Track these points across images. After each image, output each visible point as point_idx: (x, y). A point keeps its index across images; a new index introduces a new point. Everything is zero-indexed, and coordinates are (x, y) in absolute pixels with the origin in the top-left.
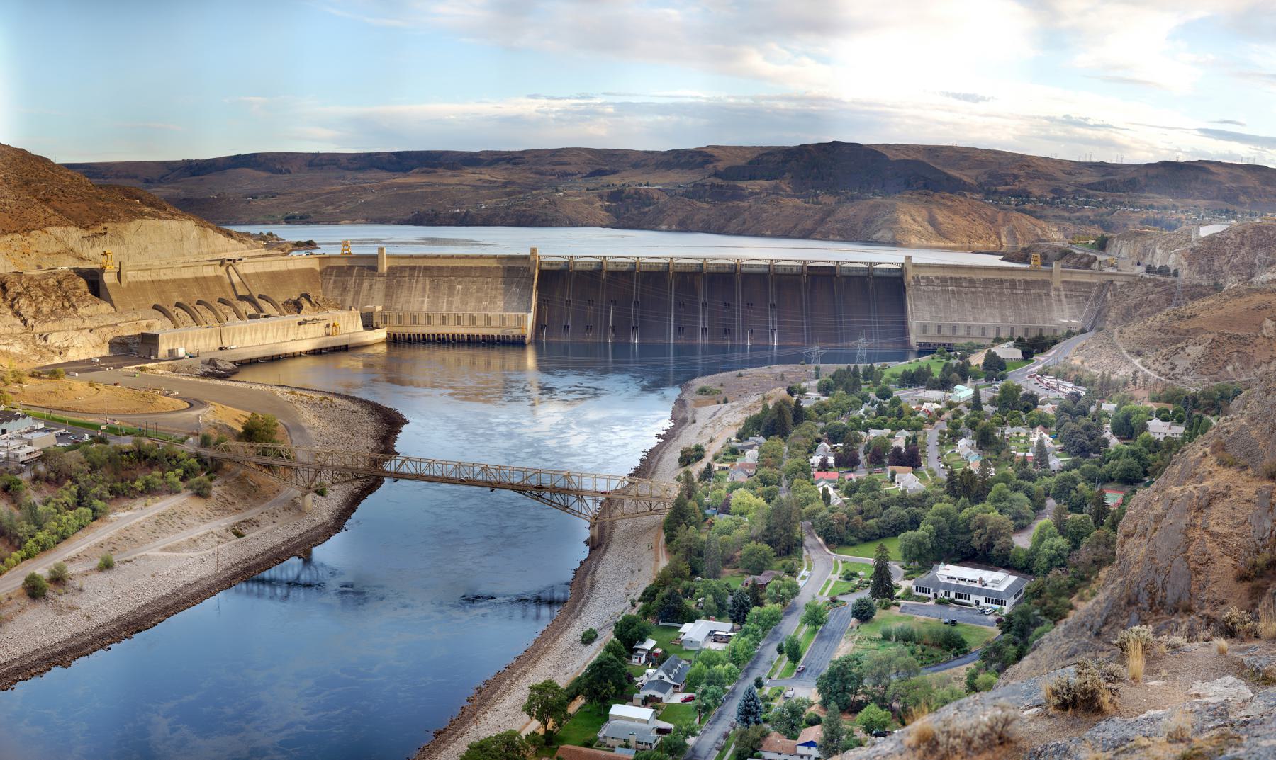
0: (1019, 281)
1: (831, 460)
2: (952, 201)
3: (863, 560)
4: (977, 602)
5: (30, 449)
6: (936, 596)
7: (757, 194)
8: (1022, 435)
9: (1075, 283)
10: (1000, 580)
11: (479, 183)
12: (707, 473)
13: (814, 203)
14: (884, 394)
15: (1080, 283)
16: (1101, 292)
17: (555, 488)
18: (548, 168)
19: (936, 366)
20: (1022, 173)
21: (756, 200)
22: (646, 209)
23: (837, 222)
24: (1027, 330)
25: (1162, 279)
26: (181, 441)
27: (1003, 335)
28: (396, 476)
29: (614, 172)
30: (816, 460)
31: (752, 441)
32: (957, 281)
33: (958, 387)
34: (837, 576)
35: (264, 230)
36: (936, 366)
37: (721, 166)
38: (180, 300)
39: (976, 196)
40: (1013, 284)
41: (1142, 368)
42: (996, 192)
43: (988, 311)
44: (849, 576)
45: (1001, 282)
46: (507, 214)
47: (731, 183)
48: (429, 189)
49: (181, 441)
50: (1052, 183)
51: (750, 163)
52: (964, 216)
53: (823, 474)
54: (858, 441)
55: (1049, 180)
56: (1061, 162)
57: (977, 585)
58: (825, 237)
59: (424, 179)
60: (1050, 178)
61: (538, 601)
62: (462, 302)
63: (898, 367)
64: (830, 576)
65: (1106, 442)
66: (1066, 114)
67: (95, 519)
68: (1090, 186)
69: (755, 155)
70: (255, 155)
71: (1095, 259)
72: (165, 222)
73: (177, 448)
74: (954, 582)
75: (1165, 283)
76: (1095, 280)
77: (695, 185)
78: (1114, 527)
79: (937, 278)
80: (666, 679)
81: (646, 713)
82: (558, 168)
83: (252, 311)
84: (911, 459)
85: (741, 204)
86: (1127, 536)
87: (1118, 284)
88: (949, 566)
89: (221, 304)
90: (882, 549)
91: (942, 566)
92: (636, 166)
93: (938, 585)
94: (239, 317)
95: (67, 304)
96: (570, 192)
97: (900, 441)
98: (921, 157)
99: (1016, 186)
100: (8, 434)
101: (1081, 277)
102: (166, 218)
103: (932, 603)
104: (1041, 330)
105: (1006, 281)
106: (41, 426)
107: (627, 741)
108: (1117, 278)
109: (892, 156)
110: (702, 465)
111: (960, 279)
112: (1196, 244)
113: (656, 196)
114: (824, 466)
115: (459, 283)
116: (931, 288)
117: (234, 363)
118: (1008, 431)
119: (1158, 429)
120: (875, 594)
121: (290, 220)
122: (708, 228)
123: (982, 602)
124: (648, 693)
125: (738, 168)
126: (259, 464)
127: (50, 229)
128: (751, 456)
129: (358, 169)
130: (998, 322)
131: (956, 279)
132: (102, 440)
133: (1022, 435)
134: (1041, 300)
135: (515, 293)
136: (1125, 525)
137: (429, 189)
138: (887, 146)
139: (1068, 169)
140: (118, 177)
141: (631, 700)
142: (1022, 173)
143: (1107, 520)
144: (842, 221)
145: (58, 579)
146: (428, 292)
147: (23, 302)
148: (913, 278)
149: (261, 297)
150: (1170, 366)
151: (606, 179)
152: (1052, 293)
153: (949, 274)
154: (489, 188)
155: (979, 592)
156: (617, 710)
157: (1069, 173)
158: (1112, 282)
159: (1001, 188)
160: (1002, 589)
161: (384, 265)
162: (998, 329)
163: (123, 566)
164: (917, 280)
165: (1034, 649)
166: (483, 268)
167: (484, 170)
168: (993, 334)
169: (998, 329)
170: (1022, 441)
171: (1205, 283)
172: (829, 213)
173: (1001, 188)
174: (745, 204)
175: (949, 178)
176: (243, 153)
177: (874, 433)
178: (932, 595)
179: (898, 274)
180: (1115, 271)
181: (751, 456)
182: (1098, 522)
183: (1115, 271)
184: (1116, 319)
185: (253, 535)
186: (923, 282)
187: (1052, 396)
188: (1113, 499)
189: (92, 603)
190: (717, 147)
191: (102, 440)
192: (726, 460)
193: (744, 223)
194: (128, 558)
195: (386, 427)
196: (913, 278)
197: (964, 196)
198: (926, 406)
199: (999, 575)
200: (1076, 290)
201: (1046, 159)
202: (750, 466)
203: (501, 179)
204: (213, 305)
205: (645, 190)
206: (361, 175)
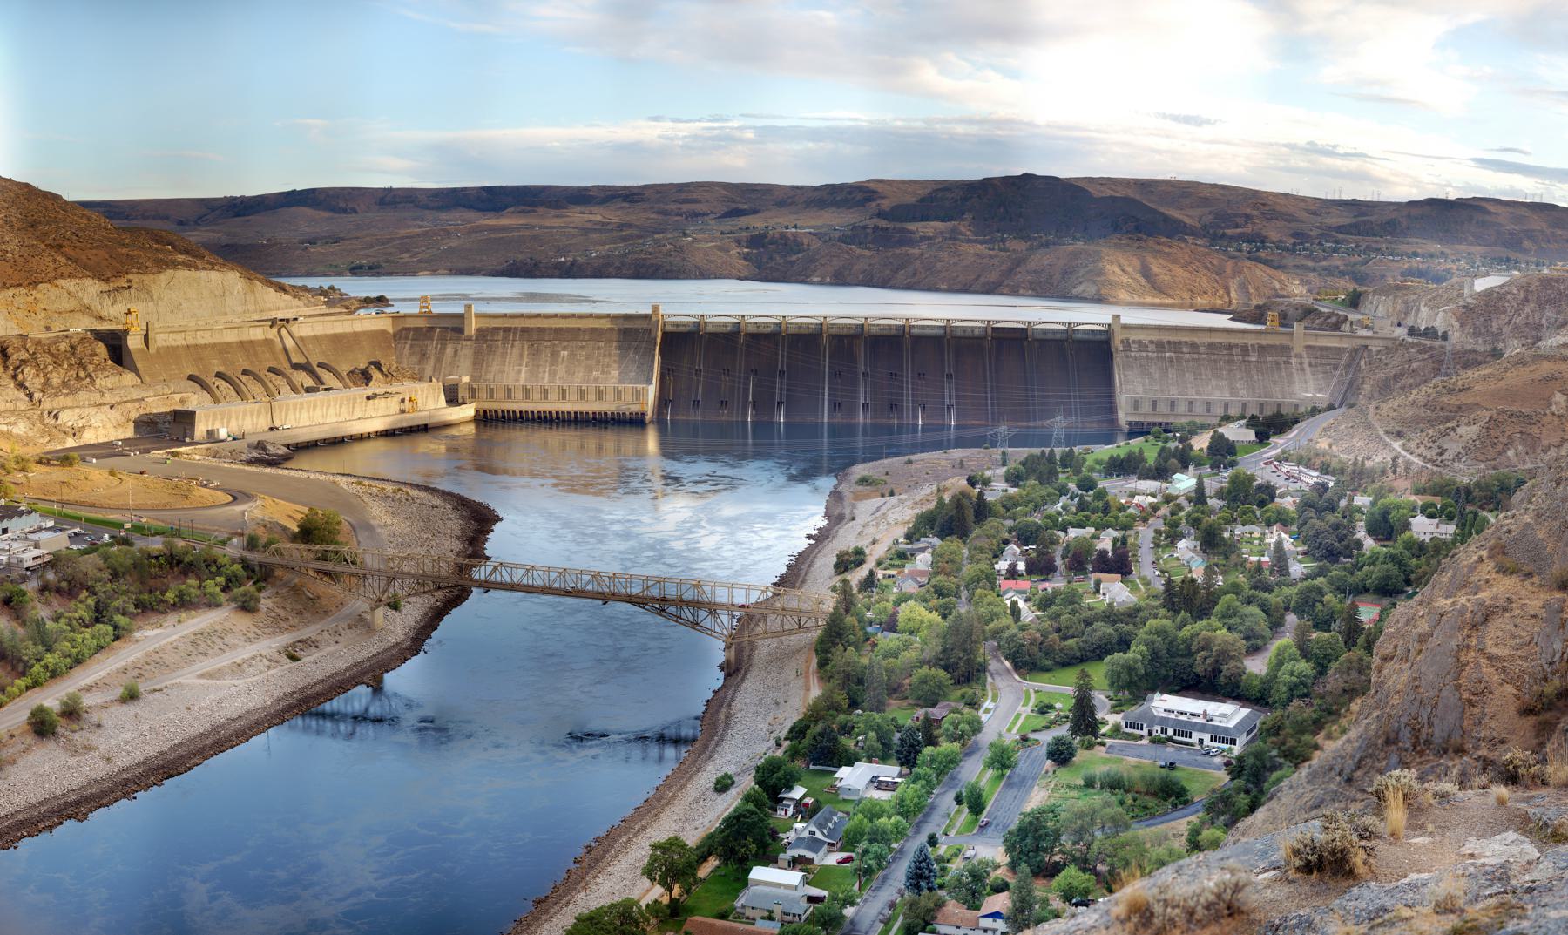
0: (1253, 346)
1: (1021, 566)
2: (1170, 247)
3: (1061, 689)
4: (1201, 741)
5: (36, 552)
6: (1150, 733)
7: (930, 238)
8: (1256, 535)
9: (1321, 349)
11: (589, 226)
12: (869, 582)
13: (1000, 250)
15: (1327, 349)
16: (1354, 359)
17: (682, 601)
18: (673, 206)
19: (1150, 450)
20: (1255, 213)
21: (929, 246)
22: (794, 258)
23: (1029, 273)
25: (1428, 343)
27: (1233, 412)
28: (487, 586)
30: (1002, 565)
31: (923, 542)
32: (1176, 346)
33: (1178, 476)
34: (1028, 709)
36: (1150, 450)
37: (886, 204)
38: (221, 369)
39: (1200, 242)
40: (1245, 350)
41: (1403, 453)
43: (1214, 382)
45: (1230, 347)
46: (623, 263)
47: (898, 225)
48: (527, 233)
49: (223, 543)
50: (1292, 225)
51: (922, 200)
52: (1185, 266)
53: (1011, 583)
55: (1289, 221)
56: (1303, 199)
57: (1201, 720)
58: (1014, 292)
59: (521, 220)
60: (1290, 218)
61: (662, 739)
63: (1104, 452)
64: (1020, 709)
69: (929, 190)
70: (313, 191)
71: (1346, 318)
72: (203, 274)
73: (217, 551)
74: (1172, 716)
75: (1431, 348)
76: (1345, 344)
77: (854, 228)
78: (1369, 648)
79: (1151, 342)
80: (819, 835)
81: (794, 877)
82: (685, 207)
83: (309, 382)
85: (911, 251)
86: (1385, 659)
87: (1374, 349)
88: (1166, 696)
89: (271, 375)
90: (1084, 675)
91: (1157, 696)
92: (781, 204)
94: (294, 389)
95: (82, 374)
96: (700, 236)
97: (1105, 543)
98: (1131, 193)
99: (1249, 229)
101: (1328, 341)
102: (204, 269)
103: (1145, 742)
104: (1279, 406)
105: (1237, 346)
106: (51, 524)
108: (1373, 342)
109: (1096, 192)
110: (862, 572)
111: (1180, 343)
112: (1469, 300)
113: (806, 241)
114: (1012, 573)
115: (565, 348)
117: (288, 446)
118: (1239, 530)
119: (1423, 528)
120: (1075, 731)
121: (356, 271)
122: (870, 281)
123: (1207, 741)
124: (796, 852)
126: (318, 571)
127: (61, 282)
128: (923, 561)
129: (440, 208)
131: (1174, 343)
132: (126, 542)
133: (1256, 535)
134: (1279, 369)
136: (1383, 646)
137: (527, 233)
138: (1090, 180)
140: (145, 218)
141: (776, 861)
143: (1361, 640)
144: (1035, 272)
145: (71, 712)
146: (526, 360)
148: (1122, 342)
149: (320, 365)
151: (744, 221)
152: (1293, 360)
153: (1166, 337)
154: (600, 231)
155: (1202, 728)
156: (758, 873)
157: (1314, 213)
159: (1229, 232)
160: (1231, 724)
161: (472, 326)
163: (151, 697)
164: (1127, 344)
166: (593, 330)
167: (595, 209)
171: (1480, 348)
172: (1020, 262)
173: (1229, 232)
174: (916, 251)
175: (1166, 219)
176: (299, 188)
177: (1073, 533)
178: (1145, 732)
179: (1103, 337)
180: (1370, 333)
181: (923, 561)
183: (1370, 333)
185: (311, 659)
186: (1134, 347)
187: (1293, 487)
188: (1368, 613)
189: (113, 742)
193: (915, 274)
194: (157, 687)
197: (1185, 241)
199: (1228, 708)
201: (1286, 195)
202: (922, 573)
204: (261, 375)
206: (443, 216)
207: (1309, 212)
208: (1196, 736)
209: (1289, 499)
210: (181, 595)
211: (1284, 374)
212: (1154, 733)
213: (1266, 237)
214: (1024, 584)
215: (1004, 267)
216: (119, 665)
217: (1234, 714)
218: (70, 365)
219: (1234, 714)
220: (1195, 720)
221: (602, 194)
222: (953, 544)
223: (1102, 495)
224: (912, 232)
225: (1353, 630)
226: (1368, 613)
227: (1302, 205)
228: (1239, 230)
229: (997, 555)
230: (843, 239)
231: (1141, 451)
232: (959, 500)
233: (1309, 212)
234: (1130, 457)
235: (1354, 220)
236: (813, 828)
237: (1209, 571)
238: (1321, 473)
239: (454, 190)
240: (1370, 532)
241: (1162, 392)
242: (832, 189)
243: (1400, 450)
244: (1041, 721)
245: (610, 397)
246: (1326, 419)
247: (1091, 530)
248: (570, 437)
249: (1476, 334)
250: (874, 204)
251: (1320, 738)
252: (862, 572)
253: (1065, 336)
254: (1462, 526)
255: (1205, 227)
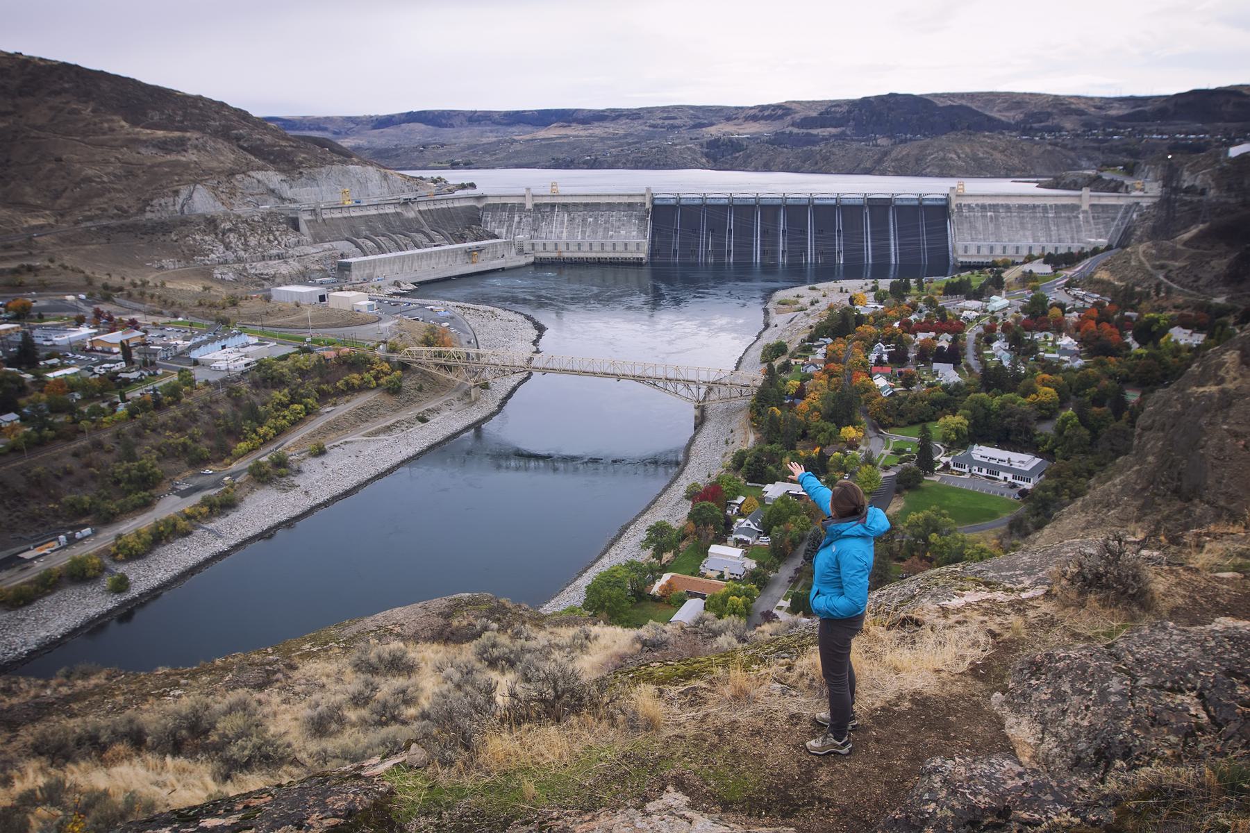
0: (1051, 206)
1: (885, 358)
2: (992, 138)
3: (908, 439)
4: (1006, 479)
5: (246, 361)
6: (970, 471)
7: (827, 139)
8: (1051, 339)
9: (1103, 206)
10: (1025, 461)
11: (605, 135)
12: (786, 367)
13: (873, 145)
14: (931, 303)
15: (1107, 206)
16: (1127, 213)
18: (660, 122)
19: (977, 280)
20: (1055, 111)
21: (826, 144)
22: (737, 155)
23: (892, 161)
24: (1056, 249)
25: (1188, 198)
26: (374, 348)
27: (1035, 253)
28: (545, 371)
29: (712, 124)
30: (873, 357)
31: (821, 341)
32: (994, 208)
33: (994, 297)
34: (888, 451)
35: (435, 174)
36: (977, 280)
37: (798, 117)
39: (1014, 134)
40: (1045, 209)
41: (1165, 281)
42: (1031, 128)
43: (1021, 233)
44: (898, 452)
45: (1034, 207)
46: (627, 160)
48: (565, 140)
49: (374, 348)
50: (1083, 117)
51: (821, 114)
52: (1002, 152)
53: (879, 368)
54: (910, 342)
55: (1081, 115)
56: (1092, 99)
57: (1006, 464)
58: (883, 173)
59: (563, 132)
60: (1080, 113)
61: (655, 462)
62: (594, 232)
63: (941, 281)
64: (883, 451)
65: (1128, 347)
66: (274, 538)
67: (308, 414)
68: (1120, 118)
69: (824, 108)
70: (425, 112)
71: (1123, 183)
73: (369, 354)
74: (986, 460)
75: (1191, 202)
76: (1122, 202)
77: (777, 134)
78: (1132, 422)
80: (752, 526)
81: (737, 552)
82: (667, 122)
84: (953, 356)
85: (814, 148)
86: (1144, 429)
87: (1145, 205)
88: (982, 447)
90: (925, 431)
91: (976, 447)
92: (728, 119)
93: (973, 462)
95: (272, 238)
96: (676, 142)
97: (944, 341)
98: (964, 102)
99: (1049, 123)
100: (227, 350)
101: (1108, 199)
103: (967, 476)
104: (1069, 248)
105: (1039, 206)
106: (256, 341)
107: (722, 572)
108: (1144, 200)
109: (940, 103)
110: (782, 360)
111: (997, 205)
112: (1225, 164)
113: (745, 143)
114: (879, 361)
115: (591, 217)
116: (972, 214)
117: (414, 284)
118: (1038, 336)
119: (1181, 336)
120: (919, 463)
121: (454, 166)
122: (787, 168)
123: (1010, 478)
124: (739, 536)
125: (813, 119)
126: (437, 365)
127: (252, 173)
128: (820, 354)
129: (509, 125)
130: (1030, 242)
131: (994, 205)
132: (308, 351)
133: (1051, 339)
134: (1070, 222)
135: (635, 224)
136: (1142, 420)
137: (565, 140)
138: (936, 95)
139: (1099, 104)
140: (311, 129)
141: (726, 541)
142: (1055, 111)
143: (1126, 415)
144: (897, 160)
145: (280, 462)
147: (232, 237)
148: (957, 205)
150: (1193, 279)
152: (1081, 216)
153: (988, 202)
154: (612, 139)
155: (1007, 470)
156: (714, 549)
157: (1100, 108)
158: (1137, 204)
159: (1035, 125)
160: (1028, 469)
162: (1030, 248)
163: (332, 451)
164: (959, 207)
165: (1055, 519)
166: (609, 204)
167: (607, 124)
168: (1025, 253)
169: (1030, 248)
170: (1050, 344)
171: (1232, 201)
172: (886, 154)
173: (1035, 125)
174: (817, 148)
175: (990, 119)
176: (415, 110)
177: (921, 336)
178: (966, 470)
179: (943, 203)
180: (1141, 194)
181: (820, 354)
182: (1117, 414)
183: (1141, 194)
184: (1141, 237)
185: (435, 420)
186: (965, 210)
187: (1079, 304)
188: (1132, 396)
189: (309, 481)
190: (794, 102)
191: (308, 351)
192: (800, 357)
193: (816, 163)
194: (336, 444)
195: (537, 332)
196: (957, 205)
197: (1003, 134)
198: (965, 313)
199: (1026, 457)
200: (1103, 211)
201: (1078, 97)
202: (820, 361)
203: (622, 132)
205: (737, 139)
206: (511, 129)
207: (1095, 107)
208: (1002, 475)
209: (1076, 314)
210: (347, 384)
211: (1074, 225)
212: (973, 472)
213: (1063, 128)
214: (887, 369)
215: (876, 157)
216: (309, 432)
217: (1030, 461)
218: (263, 232)
219: (1030, 461)
220: (1001, 463)
221: (613, 114)
222: (840, 346)
223: (941, 310)
224: (815, 136)
225: (1120, 406)
226: (1132, 396)
227: (1091, 103)
228: (1043, 124)
229: (869, 348)
230: (771, 142)
231: (969, 279)
232: (845, 314)
233: (1095, 107)
234: (961, 282)
235: (1132, 111)
236: (748, 522)
237: (1014, 364)
238: (1002, 288)
239: (517, 112)
240: (1136, 338)
241: (985, 240)
242: (763, 108)
243: (1161, 277)
244: (895, 460)
245: (609, 248)
246: (1102, 258)
247: (933, 334)
248: (596, 271)
249: (1230, 188)
250: (789, 118)
251: (1092, 482)
252: (782, 360)
253: (916, 203)
254: (1210, 336)
255: (1017, 123)
